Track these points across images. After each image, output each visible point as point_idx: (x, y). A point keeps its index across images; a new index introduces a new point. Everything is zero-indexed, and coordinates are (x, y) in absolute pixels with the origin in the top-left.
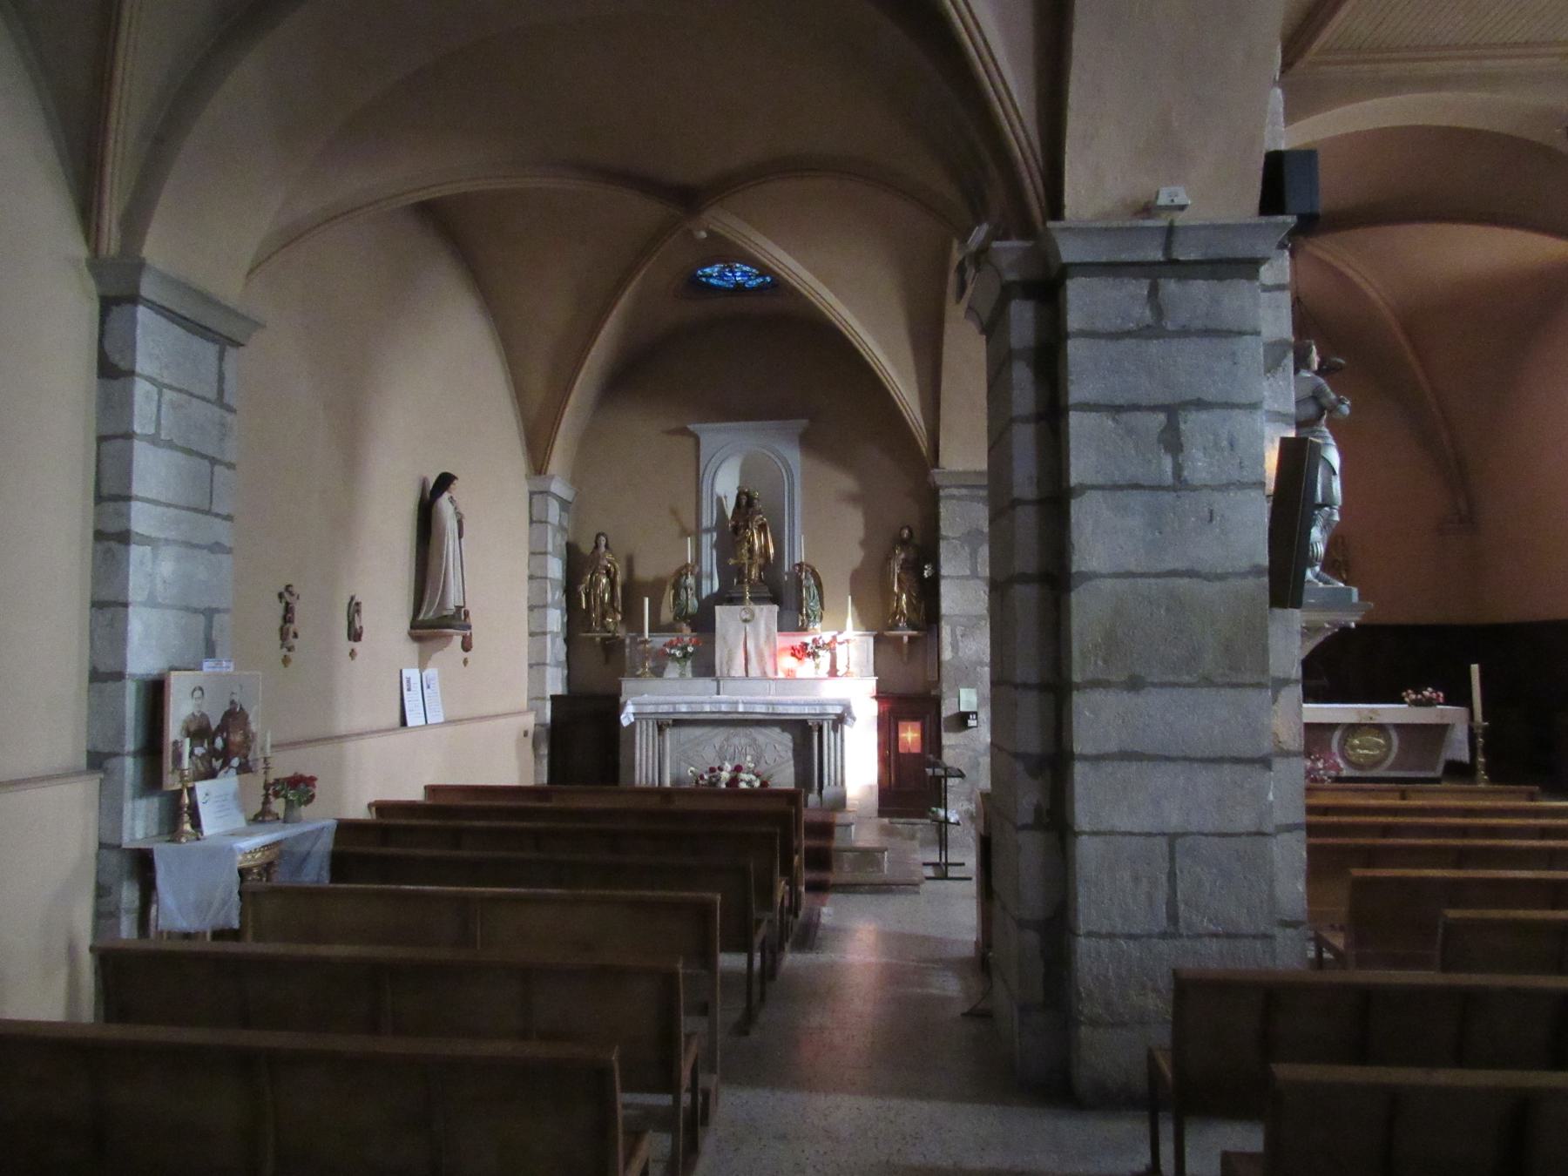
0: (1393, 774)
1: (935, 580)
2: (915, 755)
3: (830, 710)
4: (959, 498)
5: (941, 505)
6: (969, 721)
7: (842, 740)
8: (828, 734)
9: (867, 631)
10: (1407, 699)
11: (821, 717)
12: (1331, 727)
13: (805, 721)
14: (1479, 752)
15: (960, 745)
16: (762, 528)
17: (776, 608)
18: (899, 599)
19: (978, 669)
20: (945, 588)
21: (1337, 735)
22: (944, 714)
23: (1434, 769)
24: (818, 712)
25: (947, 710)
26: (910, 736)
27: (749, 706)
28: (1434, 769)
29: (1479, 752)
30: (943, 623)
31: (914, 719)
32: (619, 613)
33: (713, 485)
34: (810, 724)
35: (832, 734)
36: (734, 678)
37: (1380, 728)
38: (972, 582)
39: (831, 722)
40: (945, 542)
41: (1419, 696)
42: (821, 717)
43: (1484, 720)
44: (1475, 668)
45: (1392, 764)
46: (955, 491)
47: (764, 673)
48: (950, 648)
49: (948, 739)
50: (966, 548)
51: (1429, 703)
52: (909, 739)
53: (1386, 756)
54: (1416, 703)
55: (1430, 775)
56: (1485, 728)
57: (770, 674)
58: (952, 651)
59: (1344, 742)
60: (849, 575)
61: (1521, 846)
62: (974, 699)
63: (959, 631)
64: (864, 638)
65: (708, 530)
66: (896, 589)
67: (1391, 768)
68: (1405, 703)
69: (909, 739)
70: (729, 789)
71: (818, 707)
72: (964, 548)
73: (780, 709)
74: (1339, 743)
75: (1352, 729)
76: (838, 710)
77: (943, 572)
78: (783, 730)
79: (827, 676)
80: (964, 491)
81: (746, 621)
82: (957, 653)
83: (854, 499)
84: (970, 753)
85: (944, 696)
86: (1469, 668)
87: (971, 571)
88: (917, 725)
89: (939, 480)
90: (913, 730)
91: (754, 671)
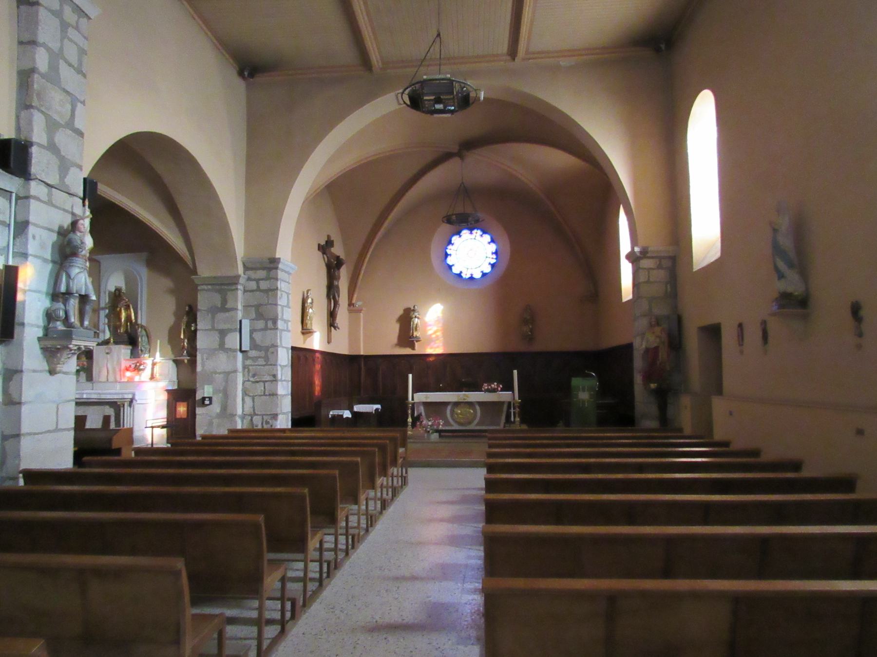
0: (478, 428)
1: (196, 331)
2: (184, 419)
3: (126, 396)
4: (208, 290)
5: (199, 294)
6: (205, 402)
7: (133, 411)
8: (127, 409)
9: (164, 357)
10: (483, 389)
11: (124, 400)
12: (445, 404)
13: (116, 402)
14: (517, 415)
15: (204, 413)
16: (127, 308)
17: (130, 347)
18: (184, 342)
19: (214, 375)
20: (199, 335)
21: (449, 408)
22: (197, 399)
23: (499, 425)
24: (121, 398)
25: (199, 396)
26: (182, 409)
27: (88, 395)
28: (499, 425)
29: (517, 415)
30: (198, 353)
31: (183, 401)
32: (185, 349)
33: (106, 285)
34: (119, 403)
35: (129, 408)
36: (101, 382)
37: (471, 404)
38: (212, 332)
39: (128, 402)
40: (200, 312)
41: (490, 387)
42: (124, 400)
43: (519, 399)
44: (515, 372)
45: (478, 423)
46: (205, 287)
47: (115, 378)
48: (201, 365)
49: (199, 411)
50: (209, 315)
51: (494, 391)
52: (182, 411)
53: (475, 418)
54: (488, 391)
55: (498, 428)
56: (520, 403)
57: (118, 379)
58: (202, 367)
59: (452, 412)
60: (167, 332)
61: (559, 462)
62: (211, 390)
63: (205, 356)
64: (167, 361)
65: (103, 309)
66: (182, 337)
67: (477, 424)
68: (482, 391)
69: (182, 411)
70: (203, 440)
71: (121, 395)
72: (208, 315)
73: (103, 397)
74: (451, 412)
75: (456, 404)
76: (130, 396)
77: (198, 327)
78: (111, 407)
79: (148, 380)
80: (210, 287)
81: (107, 353)
82: (204, 367)
83: (172, 292)
84: (209, 418)
85: (198, 389)
86: (512, 373)
87: (212, 327)
88: (185, 404)
89: (197, 282)
90: (184, 406)
91: (111, 379)
